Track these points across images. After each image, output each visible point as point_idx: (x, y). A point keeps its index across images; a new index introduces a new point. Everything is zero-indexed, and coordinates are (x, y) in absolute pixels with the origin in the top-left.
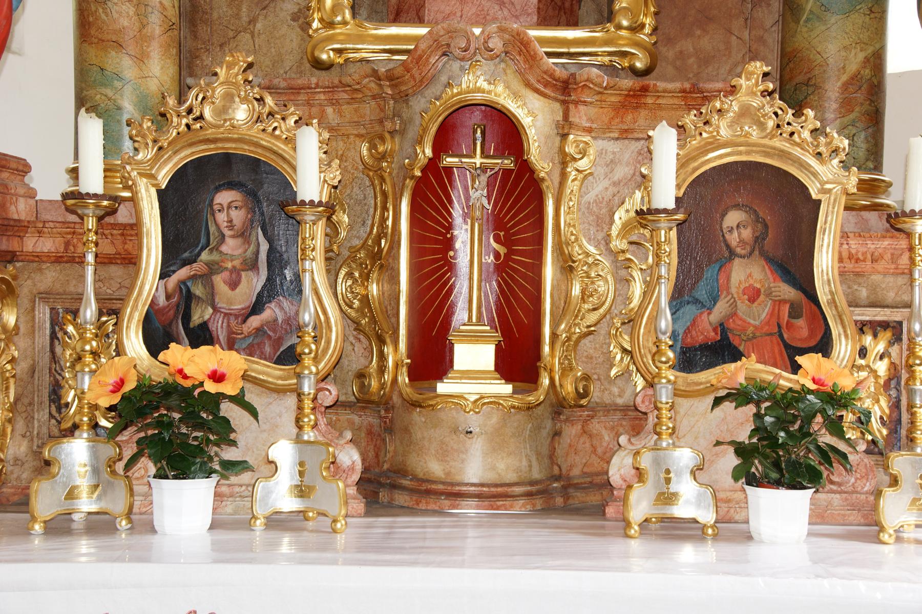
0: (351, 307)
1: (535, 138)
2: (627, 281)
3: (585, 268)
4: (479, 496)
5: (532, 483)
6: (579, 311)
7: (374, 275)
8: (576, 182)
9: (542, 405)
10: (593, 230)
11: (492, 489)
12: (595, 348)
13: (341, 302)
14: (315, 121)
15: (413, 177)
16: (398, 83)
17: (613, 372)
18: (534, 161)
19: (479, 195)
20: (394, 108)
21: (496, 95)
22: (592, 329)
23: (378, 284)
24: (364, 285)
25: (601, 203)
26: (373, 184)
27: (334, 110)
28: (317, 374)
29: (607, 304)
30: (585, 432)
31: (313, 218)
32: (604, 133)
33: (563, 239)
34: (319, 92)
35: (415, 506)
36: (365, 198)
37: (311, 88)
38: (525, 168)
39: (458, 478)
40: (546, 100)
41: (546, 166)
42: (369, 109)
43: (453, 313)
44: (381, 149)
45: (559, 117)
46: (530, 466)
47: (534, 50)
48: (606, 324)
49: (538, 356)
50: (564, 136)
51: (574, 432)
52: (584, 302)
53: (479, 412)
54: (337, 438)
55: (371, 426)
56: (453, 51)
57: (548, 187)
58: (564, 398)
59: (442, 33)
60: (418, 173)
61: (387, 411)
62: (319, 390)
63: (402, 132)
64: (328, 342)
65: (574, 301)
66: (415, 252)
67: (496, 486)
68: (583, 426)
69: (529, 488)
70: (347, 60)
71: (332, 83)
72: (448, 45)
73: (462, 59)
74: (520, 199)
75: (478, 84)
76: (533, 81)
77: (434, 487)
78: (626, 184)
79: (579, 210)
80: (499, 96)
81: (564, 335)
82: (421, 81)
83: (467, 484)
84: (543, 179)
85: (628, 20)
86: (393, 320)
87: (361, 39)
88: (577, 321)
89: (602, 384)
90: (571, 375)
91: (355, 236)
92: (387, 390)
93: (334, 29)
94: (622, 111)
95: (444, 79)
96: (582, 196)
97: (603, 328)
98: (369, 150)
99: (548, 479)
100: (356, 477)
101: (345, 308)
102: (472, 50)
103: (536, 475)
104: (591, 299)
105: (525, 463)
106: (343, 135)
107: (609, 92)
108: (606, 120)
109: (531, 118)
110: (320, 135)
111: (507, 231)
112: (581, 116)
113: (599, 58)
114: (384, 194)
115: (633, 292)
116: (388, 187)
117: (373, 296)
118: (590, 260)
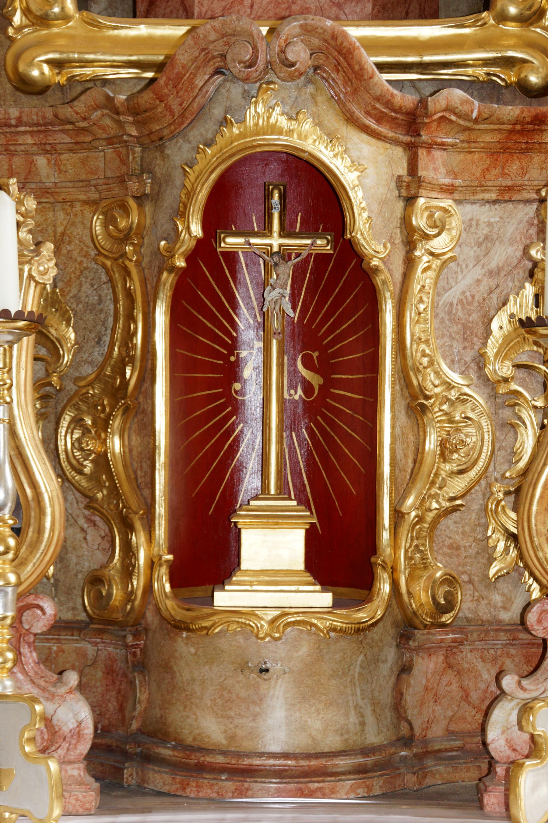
0: (80, 472)
1: (364, 205)
2: (512, 427)
3: (445, 407)
4: (281, 774)
5: (366, 751)
6: (437, 475)
7: (116, 423)
8: (429, 273)
9: (381, 624)
10: (457, 347)
11: (302, 763)
12: (464, 533)
13: (65, 464)
14: (13, 181)
15: (172, 269)
16: (154, 110)
17: (492, 571)
18: (363, 242)
19: (279, 294)
20: (142, 158)
21: (300, 137)
22: (459, 502)
23: (122, 437)
24: (99, 436)
25: (470, 304)
26: (111, 280)
27: (49, 161)
28: (19, 584)
29: (481, 463)
30: (450, 666)
31: (10, 338)
32: (475, 193)
33: (410, 362)
34: (24, 133)
35: (180, 793)
36: (100, 301)
37: (10, 126)
38: (348, 253)
39: (247, 745)
40: (380, 144)
41: (380, 248)
42: (103, 160)
43: (240, 480)
44: (123, 224)
45: (402, 170)
46: (363, 724)
47: (359, 63)
48: (480, 495)
49: (372, 547)
50: (410, 201)
51: (432, 666)
52: (445, 461)
53: (279, 638)
54: (54, 685)
55: (113, 660)
56: (231, 65)
57: (384, 282)
58: (414, 613)
59: (213, 37)
60: (181, 263)
61: (136, 635)
62: (20, 611)
63: (155, 197)
64: (40, 531)
65: (428, 460)
66: (178, 386)
67: (309, 756)
68: (446, 657)
69: (361, 760)
70: (70, 79)
71: (44, 117)
72: (223, 56)
73: (246, 80)
74: (340, 301)
75: (272, 120)
76: (359, 113)
77: (209, 759)
78: (509, 273)
79: (436, 316)
80: (306, 137)
81: (413, 514)
82: (182, 115)
83: (261, 755)
84: (376, 270)
85: (517, 4)
86: (146, 492)
87: (94, 45)
88: (433, 491)
89: (475, 589)
90: (426, 575)
91: (86, 361)
92: (137, 603)
93: (48, 26)
94: (502, 158)
95: (217, 112)
96: (439, 295)
97: (475, 502)
98: (105, 226)
99: (392, 744)
100: (84, 747)
101: (71, 473)
102: (261, 63)
103: (373, 737)
104: (455, 456)
105: (353, 719)
106: (64, 201)
107: (482, 126)
108: (478, 171)
109: (357, 173)
110: (19, 202)
111: (323, 350)
112: (435, 167)
113: (470, 71)
114: (129, 295)
115: (522, 444)
116: (136, 285)
117: (114, 454)
118: (453, 395)
